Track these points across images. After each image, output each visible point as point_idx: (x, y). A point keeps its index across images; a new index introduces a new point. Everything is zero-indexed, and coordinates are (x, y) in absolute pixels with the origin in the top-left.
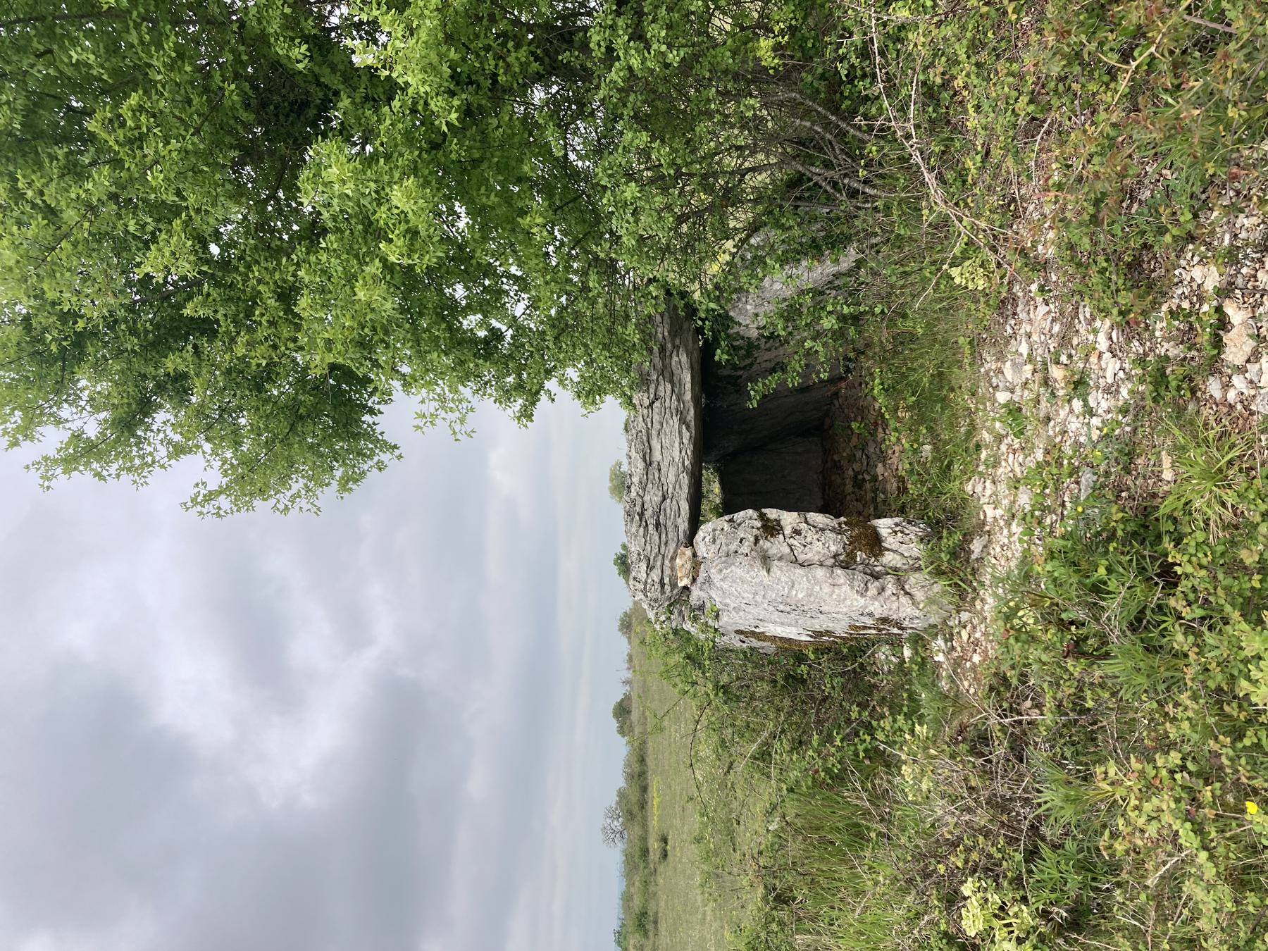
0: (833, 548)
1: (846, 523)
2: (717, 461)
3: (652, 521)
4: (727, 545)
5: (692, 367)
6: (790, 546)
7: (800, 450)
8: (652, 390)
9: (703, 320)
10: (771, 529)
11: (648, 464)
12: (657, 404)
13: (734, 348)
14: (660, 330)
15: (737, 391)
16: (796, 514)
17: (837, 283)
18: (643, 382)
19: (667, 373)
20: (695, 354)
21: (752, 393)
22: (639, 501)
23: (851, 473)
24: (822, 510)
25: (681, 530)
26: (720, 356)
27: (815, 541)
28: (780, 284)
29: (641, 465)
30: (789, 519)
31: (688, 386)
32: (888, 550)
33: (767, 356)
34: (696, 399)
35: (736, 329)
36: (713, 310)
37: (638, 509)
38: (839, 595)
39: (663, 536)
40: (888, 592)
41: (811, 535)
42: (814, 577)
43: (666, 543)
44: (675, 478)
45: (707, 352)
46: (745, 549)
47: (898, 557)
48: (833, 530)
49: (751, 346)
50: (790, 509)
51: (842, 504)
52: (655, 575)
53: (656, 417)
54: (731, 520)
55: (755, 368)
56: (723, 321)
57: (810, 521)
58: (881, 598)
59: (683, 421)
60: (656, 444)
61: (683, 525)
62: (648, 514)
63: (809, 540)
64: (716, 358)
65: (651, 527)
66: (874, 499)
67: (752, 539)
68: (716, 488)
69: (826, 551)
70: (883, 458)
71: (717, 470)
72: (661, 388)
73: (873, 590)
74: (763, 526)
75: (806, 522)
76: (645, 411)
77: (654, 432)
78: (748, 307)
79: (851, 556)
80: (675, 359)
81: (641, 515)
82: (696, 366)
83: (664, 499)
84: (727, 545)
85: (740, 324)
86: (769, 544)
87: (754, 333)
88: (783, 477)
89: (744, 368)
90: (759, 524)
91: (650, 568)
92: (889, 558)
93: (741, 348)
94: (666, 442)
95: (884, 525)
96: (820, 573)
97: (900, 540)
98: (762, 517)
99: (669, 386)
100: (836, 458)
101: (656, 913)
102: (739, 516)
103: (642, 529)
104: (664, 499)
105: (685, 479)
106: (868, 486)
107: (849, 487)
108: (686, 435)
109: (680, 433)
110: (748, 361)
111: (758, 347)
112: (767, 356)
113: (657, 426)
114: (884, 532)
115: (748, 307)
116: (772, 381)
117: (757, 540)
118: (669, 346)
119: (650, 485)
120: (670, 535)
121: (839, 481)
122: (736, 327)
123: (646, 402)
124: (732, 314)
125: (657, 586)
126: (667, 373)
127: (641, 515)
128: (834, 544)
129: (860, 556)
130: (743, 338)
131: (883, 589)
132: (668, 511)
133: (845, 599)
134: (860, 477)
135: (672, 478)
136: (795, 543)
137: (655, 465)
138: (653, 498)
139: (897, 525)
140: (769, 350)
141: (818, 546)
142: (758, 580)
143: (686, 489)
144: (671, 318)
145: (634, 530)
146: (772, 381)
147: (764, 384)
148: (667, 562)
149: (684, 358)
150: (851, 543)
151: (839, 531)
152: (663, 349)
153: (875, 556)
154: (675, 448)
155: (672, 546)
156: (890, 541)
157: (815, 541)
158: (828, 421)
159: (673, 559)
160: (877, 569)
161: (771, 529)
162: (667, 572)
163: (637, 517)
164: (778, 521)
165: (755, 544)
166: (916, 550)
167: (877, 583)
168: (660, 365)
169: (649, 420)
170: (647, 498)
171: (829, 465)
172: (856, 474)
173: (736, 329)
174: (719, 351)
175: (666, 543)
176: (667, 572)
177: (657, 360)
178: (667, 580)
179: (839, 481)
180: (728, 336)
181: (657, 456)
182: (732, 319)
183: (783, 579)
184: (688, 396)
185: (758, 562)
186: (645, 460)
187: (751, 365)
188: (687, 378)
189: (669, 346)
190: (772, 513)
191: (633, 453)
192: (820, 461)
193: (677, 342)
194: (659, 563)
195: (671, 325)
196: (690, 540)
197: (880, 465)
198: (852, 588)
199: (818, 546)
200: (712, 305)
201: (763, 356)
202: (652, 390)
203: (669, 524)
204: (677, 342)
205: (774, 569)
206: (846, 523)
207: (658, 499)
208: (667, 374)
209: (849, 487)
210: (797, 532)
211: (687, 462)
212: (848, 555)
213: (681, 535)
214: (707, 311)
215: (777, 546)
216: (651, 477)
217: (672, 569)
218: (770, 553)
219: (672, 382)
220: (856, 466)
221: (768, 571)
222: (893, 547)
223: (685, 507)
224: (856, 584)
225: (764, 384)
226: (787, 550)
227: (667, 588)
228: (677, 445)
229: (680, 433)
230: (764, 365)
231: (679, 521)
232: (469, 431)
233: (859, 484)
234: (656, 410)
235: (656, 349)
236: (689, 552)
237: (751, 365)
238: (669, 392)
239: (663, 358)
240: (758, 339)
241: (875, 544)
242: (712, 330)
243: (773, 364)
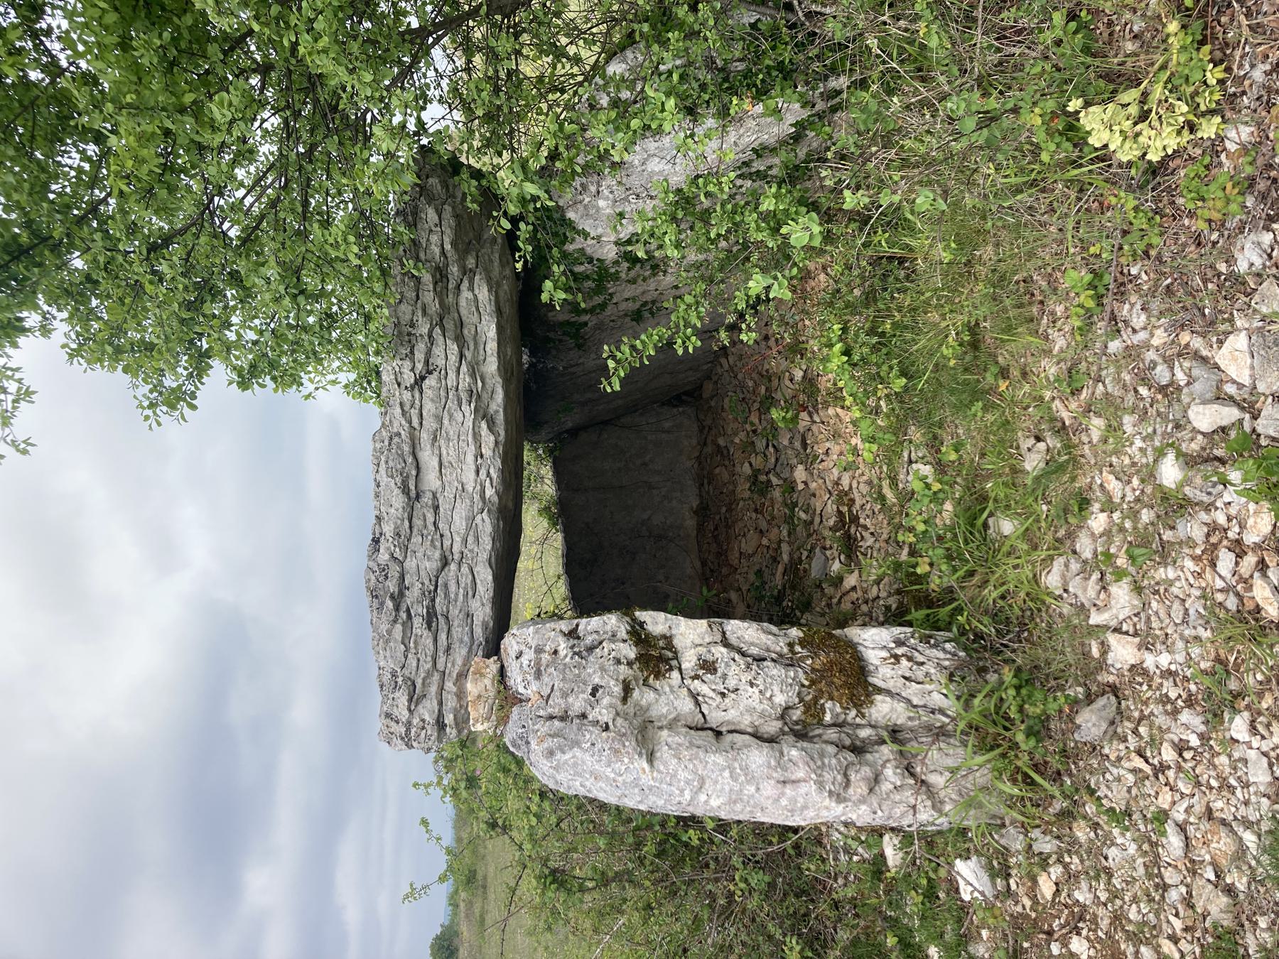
0: (780, 699)
1: (802, 643)
2: (550, 440)
3: (420, 610)
4: (565, 695)
5: (499, 311)
6: (695, 696)
7: (667, 425)
8: (419, 356)
9: (514, 221)
10: (655, 658)
11: (412, 494)
12: (431, 382)
13: (576, 277)
14: (434, 238)
15: (579, 347)
16: (704, 622)
17: (759, 165)
18: (402, 338)
19: (450, 322)
20: (505, 286)
21: (611, 364)
22: (394, 571)
23: (747, 469)
24: (752, 615)
25: (478, 621)
26: (550, 292)
27: (744, 686)
28: (664, 159)
29: (398, 500)
30: (689, 634)
31: (492, 346)
32: (880, 691)
33: (629, 291)
34: (506, 370)
35: (579, 243)
36: (535, 199)
37: (392, 586)
38: (793, 800)
39: (443, 637)
40: (886, 787)
41: (736, 673)
42: (745, 769)
43: (449, 648)
44: (467, 523)
45: (529, 282)
46: (602, 713)
47: (900, 707)
48: (779, 659)
49: (603, 275)
50: (691, 614)
51: (730, 510)
52: (427, 711)
53: (429, 407)
54: (573, 634)
55: (610, 310)
56: (554, 225)
57: (733, 640)
58: (874, 801)
59: (482, 413)
60: (429, 459)
61: (482, 611)
62: (412, 595)
63: (731, 683)
64: (545, 297)
65: (417, 622)
66: (789, 519)
67: (617, 690)
68: (547, 471)
69: (766, 706)
70: (809, 460)
71: (550, 452)
72: (438, 351)
73: (858, 788)
74: (640, 658)
75: (726, 643)
76: (407, 396)
77: (425, 437)
78: (601, 203)
79: (813, 709)
80: (466, 294)
81: (398, 599)
82: (507, 310)
83: (445, 563)
84: (565, 695)
85: (586, 235)
86: (650, 696)
87: (609, 252)
88: (645, 464)
89: (591, 311)
90: (630, 652)
91: (415, 699)
92: (883, 710)
93: (588, 277)
94: (449, 454)
95: (874, 642)
96: (758, 757)
97: (905, 674)
98: (638, 635)
99: (453, 348)
100: (721, 442)
101: (485, 878)
102: (591, 625)
103: (399, 627)
104: (445, 563)
105: (486, 524)
106: (777, 494)
107: (743, 489)
108: (488, 440)
109: (477, 436)
110: (598, 300)
111: (616, 277)
112: (629, 291)
113: (430, 423)
114: (873, 656)
115: (601, 203)
116: (649, 341)
117: (627, 689)
118: (454, 269)
119: (416, 539)
120: (457, 632)
121: (726, 476)
122: (580, 239)
123: (409, 378)
124: (571, 215)
125: (431, 730)
126: (450, 322)
127: (398, 599)
128: (777, 690)
129: (831, 709)
130: (590, 260)
131: (877, 779)
132: (453, 588)
133: (805, 807)
134: (763, 478)
135: (459, 523)
136: (704, 689)
137: (427, 499)
138: (422, 562)
139: (899, 643)
140: (633, 281)
141: (750, 697)
142: (629, 778)
143: (487, 543)
144: (457, 216)
145: (384, 627)
146: (649, 341)
147: (633, 347)
148: (449, 685)
149: (483, 293)
150: (813, 682)
151: (790, 662)
152: (440, 275)
153: (858, 706)
154: (464, 462)
155: (460, 654)
156: (884, 674)
157: (744, 686)
158: (708, 388)
159: (462, 676)
160: (864, 733)
161: (655, 658)
162: (451, 702)
163: (389, 604)
164: (668, 639)
165: (625, 700)
166: (939, 696)
167: (867, 771)
168: (434, 307)
169: (414, 413)
170: (410, 564)
171: (709, 449)
172: (756, 473)
173: (579, 243)
174: (548, 285)
175: (448, 649)
176: (451, 702)
177: (428, 297)
178: (449, 719)
179: (726, 476)
180: (565, 255)
181: (431, 480)
182: (570, 224)
183: (682, 775)
184: (492, 366)
185: (630, 744)
186: (405, 490)
187: (603, 306)
188: (490, 330)
189: (454, 269)
190: (656, 622)
191: (384, 479)
192: (694, 442)
193: (471, 263)
194: (433, 689)
195: (458, 230)
196: (493, 648)
197: (801, 467)
198: (820, 785)
199: (750, 697)
200: (531, 189)
201: (624, 294)
202: (419, 356)
203: (454, 612)
204: (471, 263)
205: (664, 753)
206: (802, 643)
207: (431, 565)
208: (449, 325)
209: (743, 489)
210: (708, 666)
211: (489, 492)
212: (808, 708)
213: (478, 631)
214: (523, 201)
215: (668, 698)
216: (417, 522)
217: (461, 694)
218: (654, 713)
219: (460, 339)
220: (757, 461)
221: (651, 758)
222: (890, 685)
223: (485, 577)
224: (828, 776)
225: (633, 347)
226: (686, 705)
227: (451, 732)
228: (470, 458)
229: (477, 436)
230: (623, 306)
231: (475, 605)
232: (20, 438)
233: (760, 486)
234: (428, 393)
235: (427, 278)
236: (492, 666)
237: (603, 306)
238: (453, 358)
239: (441, 294)
240: (616, 263)
241: (855, 681)
242: (533, 239)
243: (638, 305)
